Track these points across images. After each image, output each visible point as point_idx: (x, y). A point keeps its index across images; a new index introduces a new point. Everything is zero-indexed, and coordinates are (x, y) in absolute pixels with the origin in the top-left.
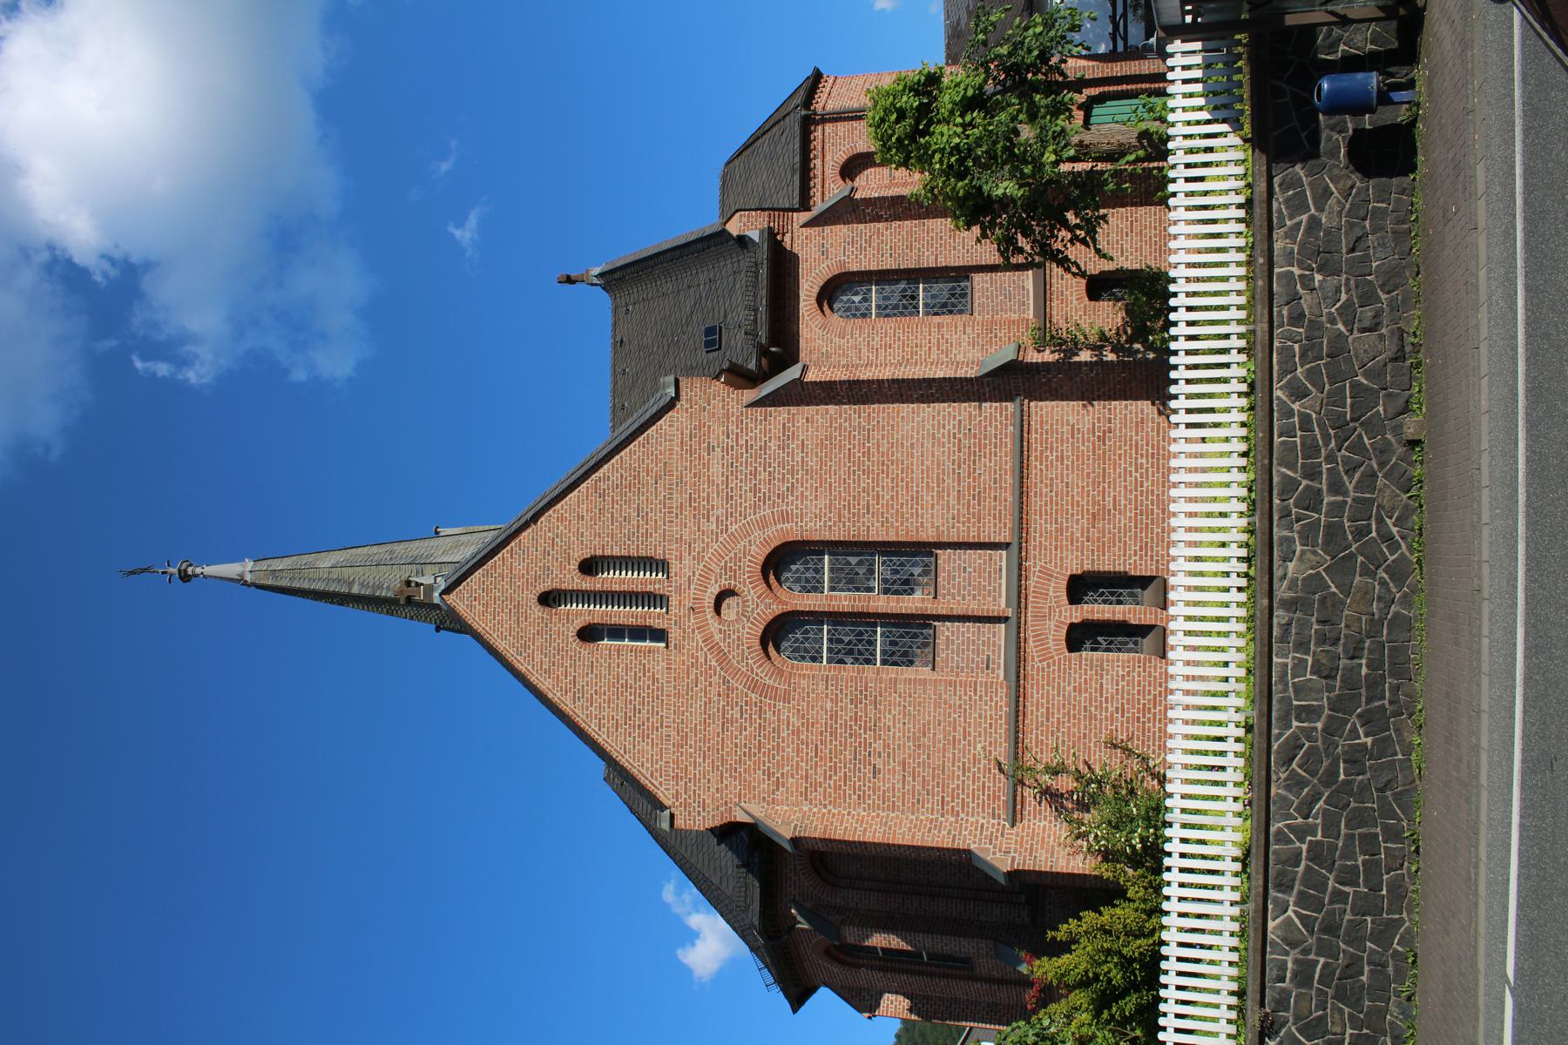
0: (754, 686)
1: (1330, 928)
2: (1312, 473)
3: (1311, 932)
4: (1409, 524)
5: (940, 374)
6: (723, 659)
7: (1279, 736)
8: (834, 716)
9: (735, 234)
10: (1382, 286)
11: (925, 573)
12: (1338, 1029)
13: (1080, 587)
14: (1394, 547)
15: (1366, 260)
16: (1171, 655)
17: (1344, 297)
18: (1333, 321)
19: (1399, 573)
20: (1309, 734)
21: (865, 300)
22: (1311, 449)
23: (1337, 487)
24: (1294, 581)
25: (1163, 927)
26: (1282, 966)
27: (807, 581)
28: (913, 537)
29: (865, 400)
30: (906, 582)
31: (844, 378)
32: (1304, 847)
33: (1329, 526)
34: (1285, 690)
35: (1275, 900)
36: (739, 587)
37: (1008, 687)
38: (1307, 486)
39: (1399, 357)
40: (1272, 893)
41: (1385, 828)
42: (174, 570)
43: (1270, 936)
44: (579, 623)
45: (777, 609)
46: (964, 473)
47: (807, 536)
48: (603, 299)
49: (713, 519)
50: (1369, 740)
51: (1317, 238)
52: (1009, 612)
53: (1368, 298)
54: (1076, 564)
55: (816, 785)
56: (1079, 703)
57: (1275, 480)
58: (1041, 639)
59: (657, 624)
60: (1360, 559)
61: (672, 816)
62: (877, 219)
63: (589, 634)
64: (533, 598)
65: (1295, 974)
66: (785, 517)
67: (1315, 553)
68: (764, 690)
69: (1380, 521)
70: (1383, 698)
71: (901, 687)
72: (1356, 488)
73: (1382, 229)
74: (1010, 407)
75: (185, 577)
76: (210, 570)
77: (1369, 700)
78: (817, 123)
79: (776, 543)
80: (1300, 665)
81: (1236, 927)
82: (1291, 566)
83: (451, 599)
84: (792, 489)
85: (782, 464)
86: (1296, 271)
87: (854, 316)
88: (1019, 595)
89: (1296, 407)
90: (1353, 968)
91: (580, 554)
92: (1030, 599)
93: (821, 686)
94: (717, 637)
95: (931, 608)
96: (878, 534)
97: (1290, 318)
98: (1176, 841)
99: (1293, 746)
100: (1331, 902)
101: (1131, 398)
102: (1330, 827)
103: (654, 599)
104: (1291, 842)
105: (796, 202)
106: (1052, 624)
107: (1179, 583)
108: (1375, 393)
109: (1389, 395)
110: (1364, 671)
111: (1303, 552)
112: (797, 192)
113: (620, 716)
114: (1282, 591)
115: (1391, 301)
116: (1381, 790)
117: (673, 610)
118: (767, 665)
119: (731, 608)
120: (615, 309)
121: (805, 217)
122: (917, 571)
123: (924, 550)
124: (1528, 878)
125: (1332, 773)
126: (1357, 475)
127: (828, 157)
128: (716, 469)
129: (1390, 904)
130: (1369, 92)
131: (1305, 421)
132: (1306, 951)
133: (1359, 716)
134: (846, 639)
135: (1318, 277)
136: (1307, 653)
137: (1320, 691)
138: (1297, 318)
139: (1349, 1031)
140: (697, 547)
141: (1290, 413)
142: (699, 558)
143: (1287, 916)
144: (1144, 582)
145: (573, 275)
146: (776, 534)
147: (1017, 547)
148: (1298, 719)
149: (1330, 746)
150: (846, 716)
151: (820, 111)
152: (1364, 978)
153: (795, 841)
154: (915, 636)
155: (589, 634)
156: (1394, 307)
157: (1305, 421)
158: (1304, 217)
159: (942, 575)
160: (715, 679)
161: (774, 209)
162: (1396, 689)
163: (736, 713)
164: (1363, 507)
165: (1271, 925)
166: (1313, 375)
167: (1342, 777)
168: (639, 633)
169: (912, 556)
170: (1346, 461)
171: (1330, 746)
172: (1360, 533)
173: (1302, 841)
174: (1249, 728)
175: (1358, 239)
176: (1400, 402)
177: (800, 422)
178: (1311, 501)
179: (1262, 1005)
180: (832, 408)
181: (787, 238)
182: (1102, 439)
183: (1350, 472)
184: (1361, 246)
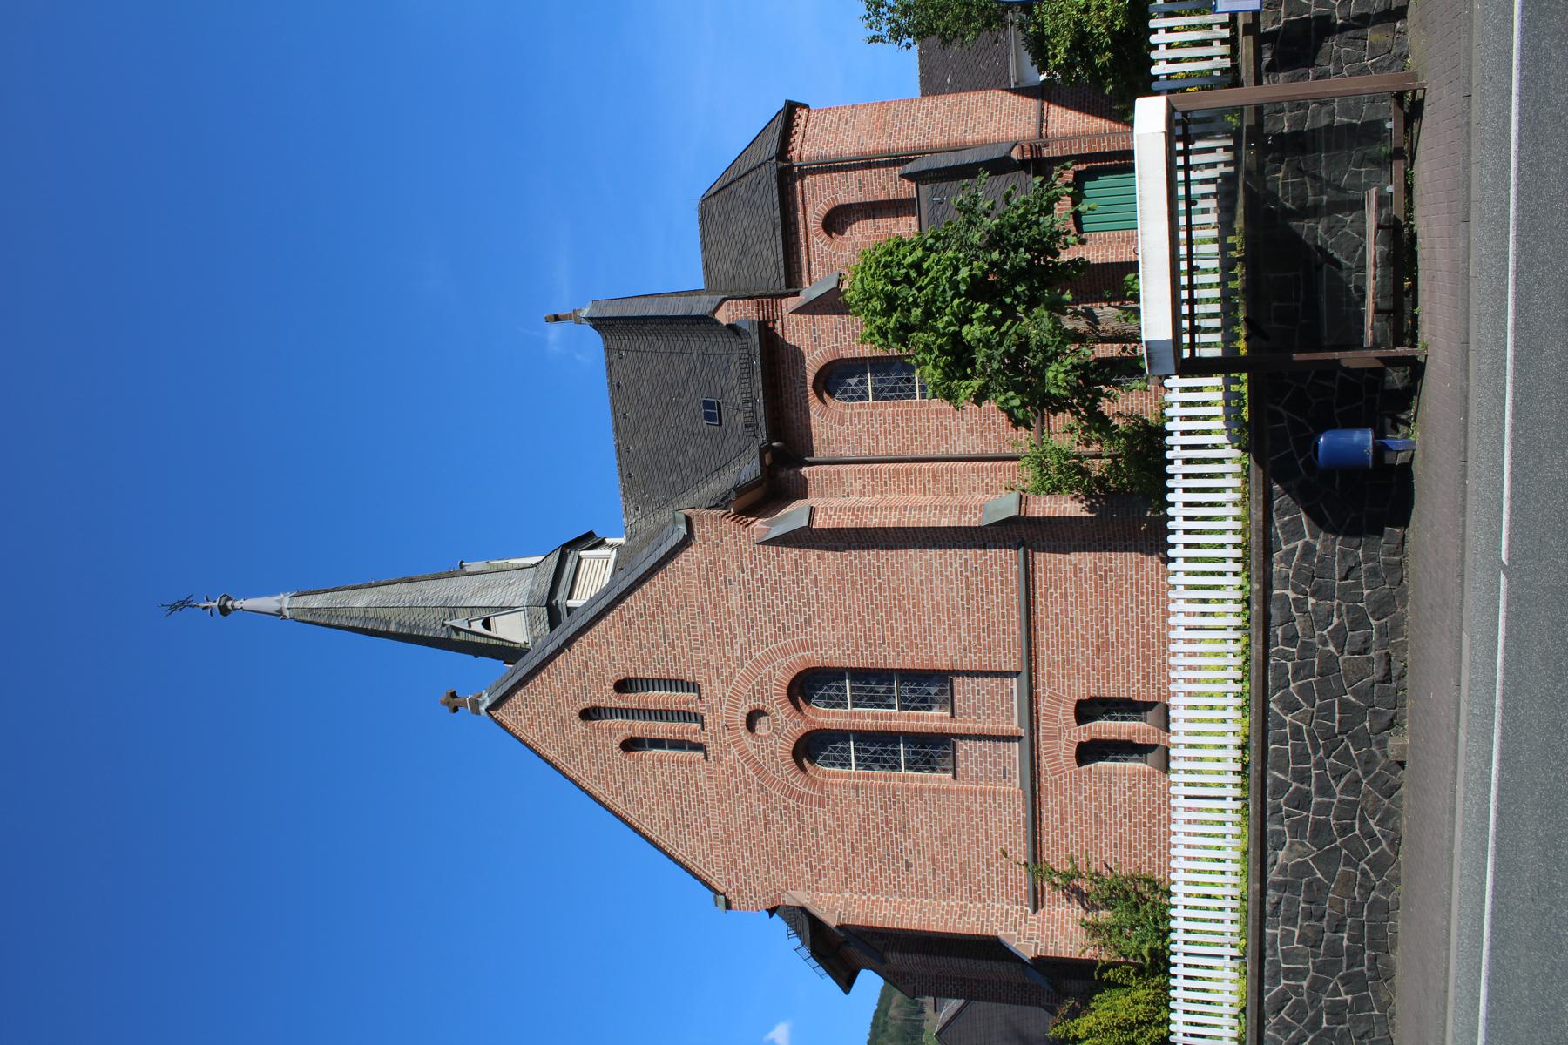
0: (791, 793)
2: (1303, 777)
5: (944, 523)
6: (759, 769)
8: (867, 819)
9: (725, 323)
10: (1373, 614)
11: (942, 692)
13: (1087, 710)
14: (1375, 843)
15: (1358, 586)
16: (1172, 727)
17: (1335, 621)
18: (1325, 643)
19: (1379, 865)
20: (1296, 990)
21: (861, 382)
22: (1302, 757)
23: (1324, 790)
24: (1283, 868)
25: (1171, 930)
27: (831, 698)
28: (927, 665)
30: (924, 700)
31: (851, 525)
33: (1316, 823)
34: (1275, 954)
38: (1297, 789)
39: (1387, 678)
44: (621, 737)
45: (805, 727)
47: (827, 663)
48: (594, 338)
49: (737, 647)
50: (1349, 998)
51: (1311, 564)
52: (1023, 732)
53: (1359, 622)
54: (1083, 690)
56: (1090, 812)
58: (1053, 756)
59: (695, 738)
60: (1344, 852)
63: (630, 745)
64: (575, 714)
66: (805, 646)
67: (1303, 845)
68: (800, 797)
69: (1363, 821)
71: (926, 795)
72: (1342, 792)
73: (1373, 560)
75: (224, 610)
76: (250, 603)
78: (802, 174)
79: (799, 669)
80: (1288, 937)
82: (1281, 854)
84: (809, 620)
85: (798, 597)
86: (1291, 594)
87: (852, 399)
89: (1288, 718)
91: (613, 676)
93: (853, 793)
94: (752, 751)
95: (949, 726)
96: (893, 661)
97: (1284, 639)
98: (1180, 932)
99: (1282, 999)
106: (1063, 743)
108: (1362, 711)
109: (1374, 713)
110: (1345, 943)
111: (1292, 844)
112: (780, 248)
114: (1273, 875)
115: (1380, 627)
117: (708, 727)
118: (801, 775)
119: (762, 727)
120: (608, 350)
122: (933, 690)
123: (943, 677)
124: (1495, 981)
125: (1316, 1023)
126: (1343, 780)
127: (809, 210)
128: (735, 601)
130: (1365, 456)
133: (1341, 978)
134: (872, 749)
135: (1311, 601)
136: (1295, 925)
137: (1306, 956)
138: (1291, 639)
140: (725, 672)
141: (1282, 724)
142: (727, 681)
144: (1148, 706)
145: (560, 312)
147: (1029, 673)
149: (1314, 1000)
150: (877, 819)
151: (796, 161)
153: (841, 927)
155: (630, 745)
156: (1383, 632)
157: (1297, 732)
158: (1300, 543)
159: (957, 697)
160: (754, 787)
161: (761, 296)
162: (1374, 959)
164: (1348, 809)
166: (1305, 691)
168: (678, 745)
169: (928, 684)
170: (1333, 768)
171: (1314, 1000)
172: (1344, 830)
175: (1351, 569)
176: (1386, 719)
178: (1301, 801)
181: (778, 325)
182: (1104, 578)
183: (1337, 778)
184: (1352, 575)
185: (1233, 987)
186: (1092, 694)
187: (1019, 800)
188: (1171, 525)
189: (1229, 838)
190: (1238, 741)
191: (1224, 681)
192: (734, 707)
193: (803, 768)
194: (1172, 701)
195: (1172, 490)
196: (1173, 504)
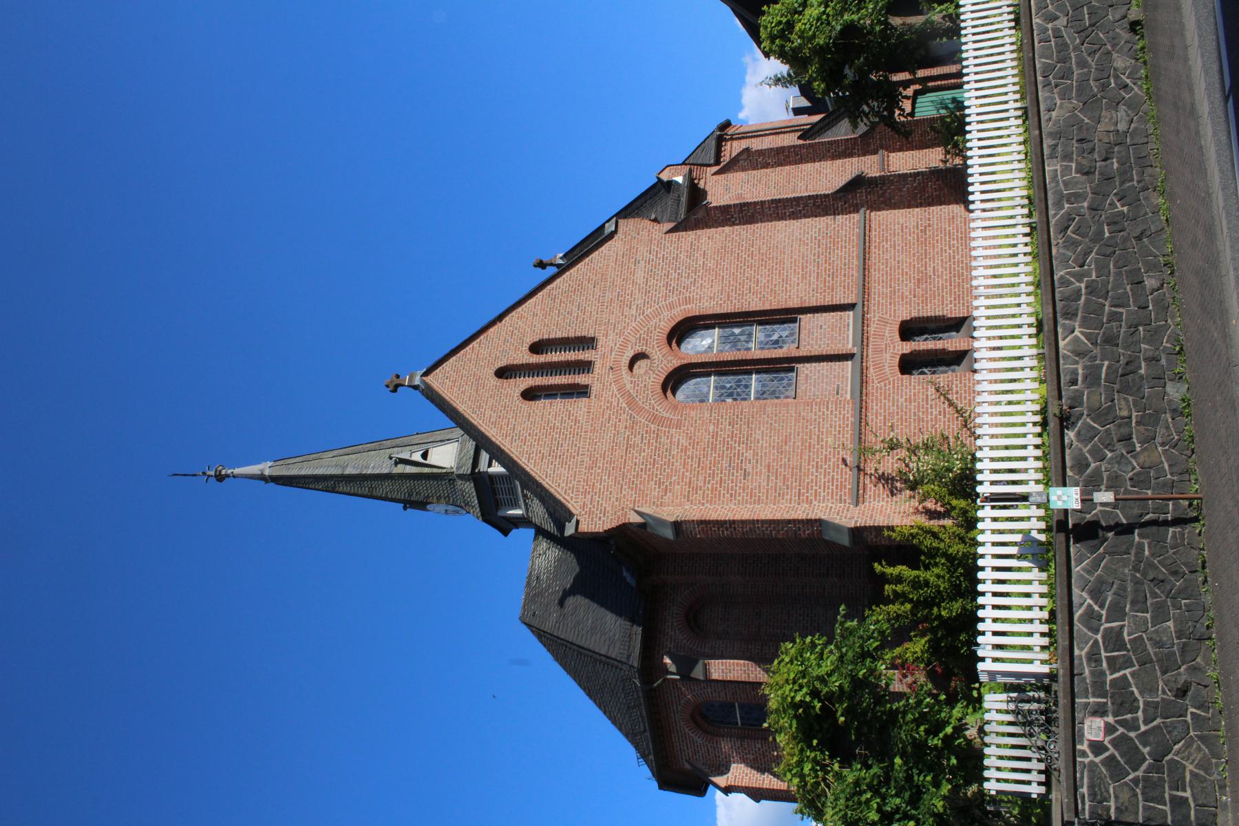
0: (655, 419)
1: (1111, 340)
3: (1095, 344)
4: (1138, 75)
6: (631, 402)
7: (1055, 215)
12: (1125, 413)
13: (909, 330)
22: (1062, 47)
26: (1075, 372)
29: (751, 220)
30: (776, 342)
32: (1083, 285)
35: (1064, 325)
36: (648, 351)
37: (854, 403)
40: (1061, 321)
41: (1146, 263)
42: (212, 473)
43: (1062, 351)
46: (822, 260)
49: (634, 307)
50: (1125, 209)
52: (855, 350)
54: (905, 314)
55: (697, 489)
57: (1038, 66)
61: (578, 522)
62: (766, 166)
65: (1085, 378)
66: (687, 301)
69: (1117, 77)
70: (1132, 180)
74: (856, 217)
75: (220, 478)
77: (1122, 183)
78: (726, 140)
80: (1067, 170)
81: (1040, 476)
82: (1054, 114)
83: (428, 379)
88: (863, 338)
90: (1131, 367)
92: (871, 339)
94: (629, 386)
100: (1109, 321)
101: (945, 203)
102: (1102, 269)
103: (586, 366)
104: (1072, 283)
105: (712, 162)
106: (888, 355)
107: (981, 312)
110: (1116, 166)
113: (545, 451)
114: (1047, 127)
116: (1139, 238)
119: (641, 365)
121: (716, 168)
128: (640, 275)
129: (1157, 314)
131: (1057, 32)
132: (1095, 358)
136: (1071, 160)
139: (1134, 414)
143: (1073, 335)
145: (545, 260)
146: (679, 314)
148: (1069, 202)
152: (1142, 371)
154: (782, 379)
160: (624, 417)
163: (638, 440)
165: (1062, 344)
167: (1107, 235)
173: (1080, 281)
174: (1038, 286)
177: (704, 239)
179: (1060, 398)
180: (727, 229)
185: (1029, 269)
186: (913, 315)
187: (849, 407)
188: (981, 613)
189: (1024, 306)
190: (1037, 408)
191: (1012, 162)
192: (621, 353)
193: (670, 345)
194: (987, 751)
195: (983, 620)
196: (983, 594)
